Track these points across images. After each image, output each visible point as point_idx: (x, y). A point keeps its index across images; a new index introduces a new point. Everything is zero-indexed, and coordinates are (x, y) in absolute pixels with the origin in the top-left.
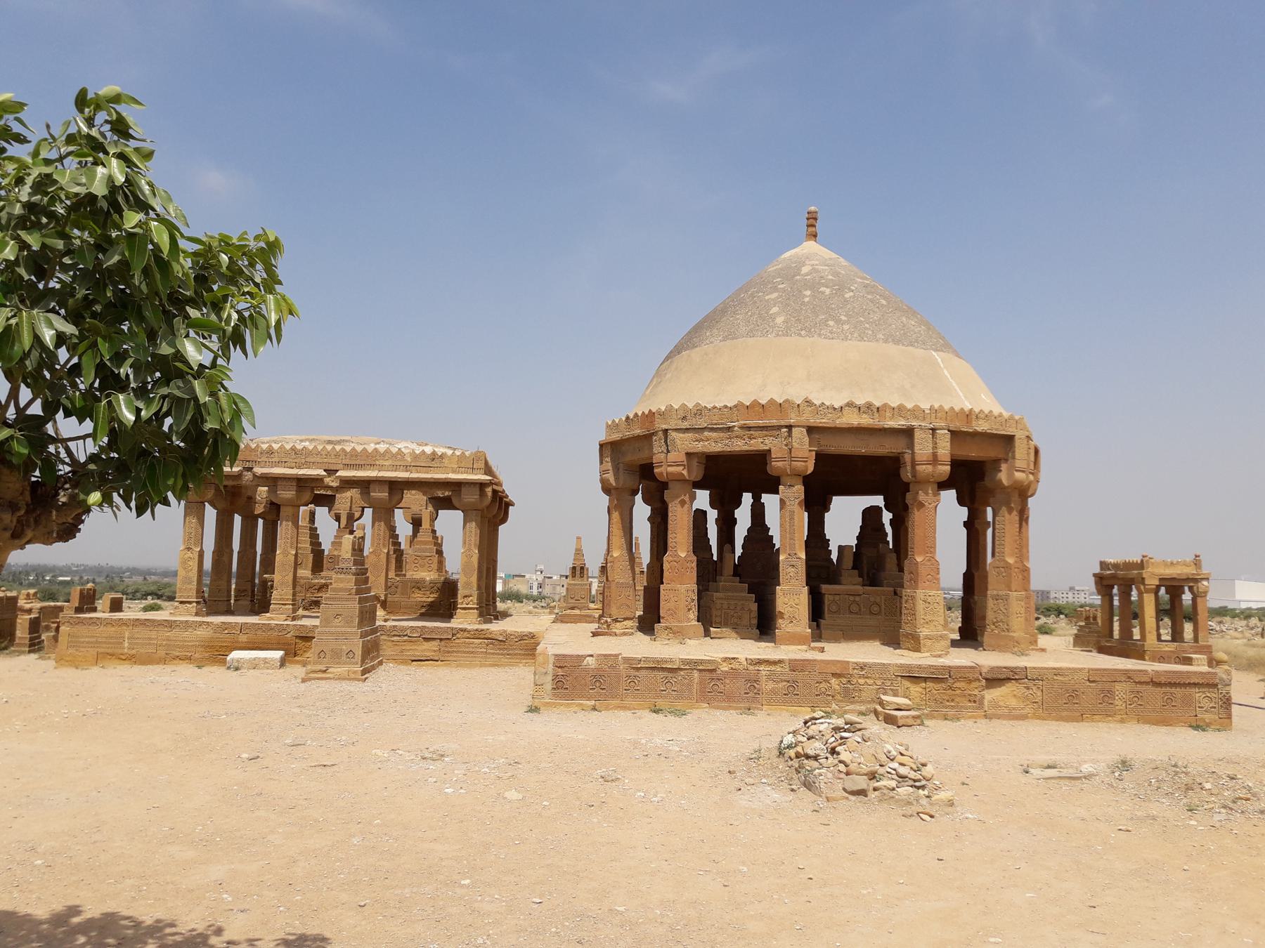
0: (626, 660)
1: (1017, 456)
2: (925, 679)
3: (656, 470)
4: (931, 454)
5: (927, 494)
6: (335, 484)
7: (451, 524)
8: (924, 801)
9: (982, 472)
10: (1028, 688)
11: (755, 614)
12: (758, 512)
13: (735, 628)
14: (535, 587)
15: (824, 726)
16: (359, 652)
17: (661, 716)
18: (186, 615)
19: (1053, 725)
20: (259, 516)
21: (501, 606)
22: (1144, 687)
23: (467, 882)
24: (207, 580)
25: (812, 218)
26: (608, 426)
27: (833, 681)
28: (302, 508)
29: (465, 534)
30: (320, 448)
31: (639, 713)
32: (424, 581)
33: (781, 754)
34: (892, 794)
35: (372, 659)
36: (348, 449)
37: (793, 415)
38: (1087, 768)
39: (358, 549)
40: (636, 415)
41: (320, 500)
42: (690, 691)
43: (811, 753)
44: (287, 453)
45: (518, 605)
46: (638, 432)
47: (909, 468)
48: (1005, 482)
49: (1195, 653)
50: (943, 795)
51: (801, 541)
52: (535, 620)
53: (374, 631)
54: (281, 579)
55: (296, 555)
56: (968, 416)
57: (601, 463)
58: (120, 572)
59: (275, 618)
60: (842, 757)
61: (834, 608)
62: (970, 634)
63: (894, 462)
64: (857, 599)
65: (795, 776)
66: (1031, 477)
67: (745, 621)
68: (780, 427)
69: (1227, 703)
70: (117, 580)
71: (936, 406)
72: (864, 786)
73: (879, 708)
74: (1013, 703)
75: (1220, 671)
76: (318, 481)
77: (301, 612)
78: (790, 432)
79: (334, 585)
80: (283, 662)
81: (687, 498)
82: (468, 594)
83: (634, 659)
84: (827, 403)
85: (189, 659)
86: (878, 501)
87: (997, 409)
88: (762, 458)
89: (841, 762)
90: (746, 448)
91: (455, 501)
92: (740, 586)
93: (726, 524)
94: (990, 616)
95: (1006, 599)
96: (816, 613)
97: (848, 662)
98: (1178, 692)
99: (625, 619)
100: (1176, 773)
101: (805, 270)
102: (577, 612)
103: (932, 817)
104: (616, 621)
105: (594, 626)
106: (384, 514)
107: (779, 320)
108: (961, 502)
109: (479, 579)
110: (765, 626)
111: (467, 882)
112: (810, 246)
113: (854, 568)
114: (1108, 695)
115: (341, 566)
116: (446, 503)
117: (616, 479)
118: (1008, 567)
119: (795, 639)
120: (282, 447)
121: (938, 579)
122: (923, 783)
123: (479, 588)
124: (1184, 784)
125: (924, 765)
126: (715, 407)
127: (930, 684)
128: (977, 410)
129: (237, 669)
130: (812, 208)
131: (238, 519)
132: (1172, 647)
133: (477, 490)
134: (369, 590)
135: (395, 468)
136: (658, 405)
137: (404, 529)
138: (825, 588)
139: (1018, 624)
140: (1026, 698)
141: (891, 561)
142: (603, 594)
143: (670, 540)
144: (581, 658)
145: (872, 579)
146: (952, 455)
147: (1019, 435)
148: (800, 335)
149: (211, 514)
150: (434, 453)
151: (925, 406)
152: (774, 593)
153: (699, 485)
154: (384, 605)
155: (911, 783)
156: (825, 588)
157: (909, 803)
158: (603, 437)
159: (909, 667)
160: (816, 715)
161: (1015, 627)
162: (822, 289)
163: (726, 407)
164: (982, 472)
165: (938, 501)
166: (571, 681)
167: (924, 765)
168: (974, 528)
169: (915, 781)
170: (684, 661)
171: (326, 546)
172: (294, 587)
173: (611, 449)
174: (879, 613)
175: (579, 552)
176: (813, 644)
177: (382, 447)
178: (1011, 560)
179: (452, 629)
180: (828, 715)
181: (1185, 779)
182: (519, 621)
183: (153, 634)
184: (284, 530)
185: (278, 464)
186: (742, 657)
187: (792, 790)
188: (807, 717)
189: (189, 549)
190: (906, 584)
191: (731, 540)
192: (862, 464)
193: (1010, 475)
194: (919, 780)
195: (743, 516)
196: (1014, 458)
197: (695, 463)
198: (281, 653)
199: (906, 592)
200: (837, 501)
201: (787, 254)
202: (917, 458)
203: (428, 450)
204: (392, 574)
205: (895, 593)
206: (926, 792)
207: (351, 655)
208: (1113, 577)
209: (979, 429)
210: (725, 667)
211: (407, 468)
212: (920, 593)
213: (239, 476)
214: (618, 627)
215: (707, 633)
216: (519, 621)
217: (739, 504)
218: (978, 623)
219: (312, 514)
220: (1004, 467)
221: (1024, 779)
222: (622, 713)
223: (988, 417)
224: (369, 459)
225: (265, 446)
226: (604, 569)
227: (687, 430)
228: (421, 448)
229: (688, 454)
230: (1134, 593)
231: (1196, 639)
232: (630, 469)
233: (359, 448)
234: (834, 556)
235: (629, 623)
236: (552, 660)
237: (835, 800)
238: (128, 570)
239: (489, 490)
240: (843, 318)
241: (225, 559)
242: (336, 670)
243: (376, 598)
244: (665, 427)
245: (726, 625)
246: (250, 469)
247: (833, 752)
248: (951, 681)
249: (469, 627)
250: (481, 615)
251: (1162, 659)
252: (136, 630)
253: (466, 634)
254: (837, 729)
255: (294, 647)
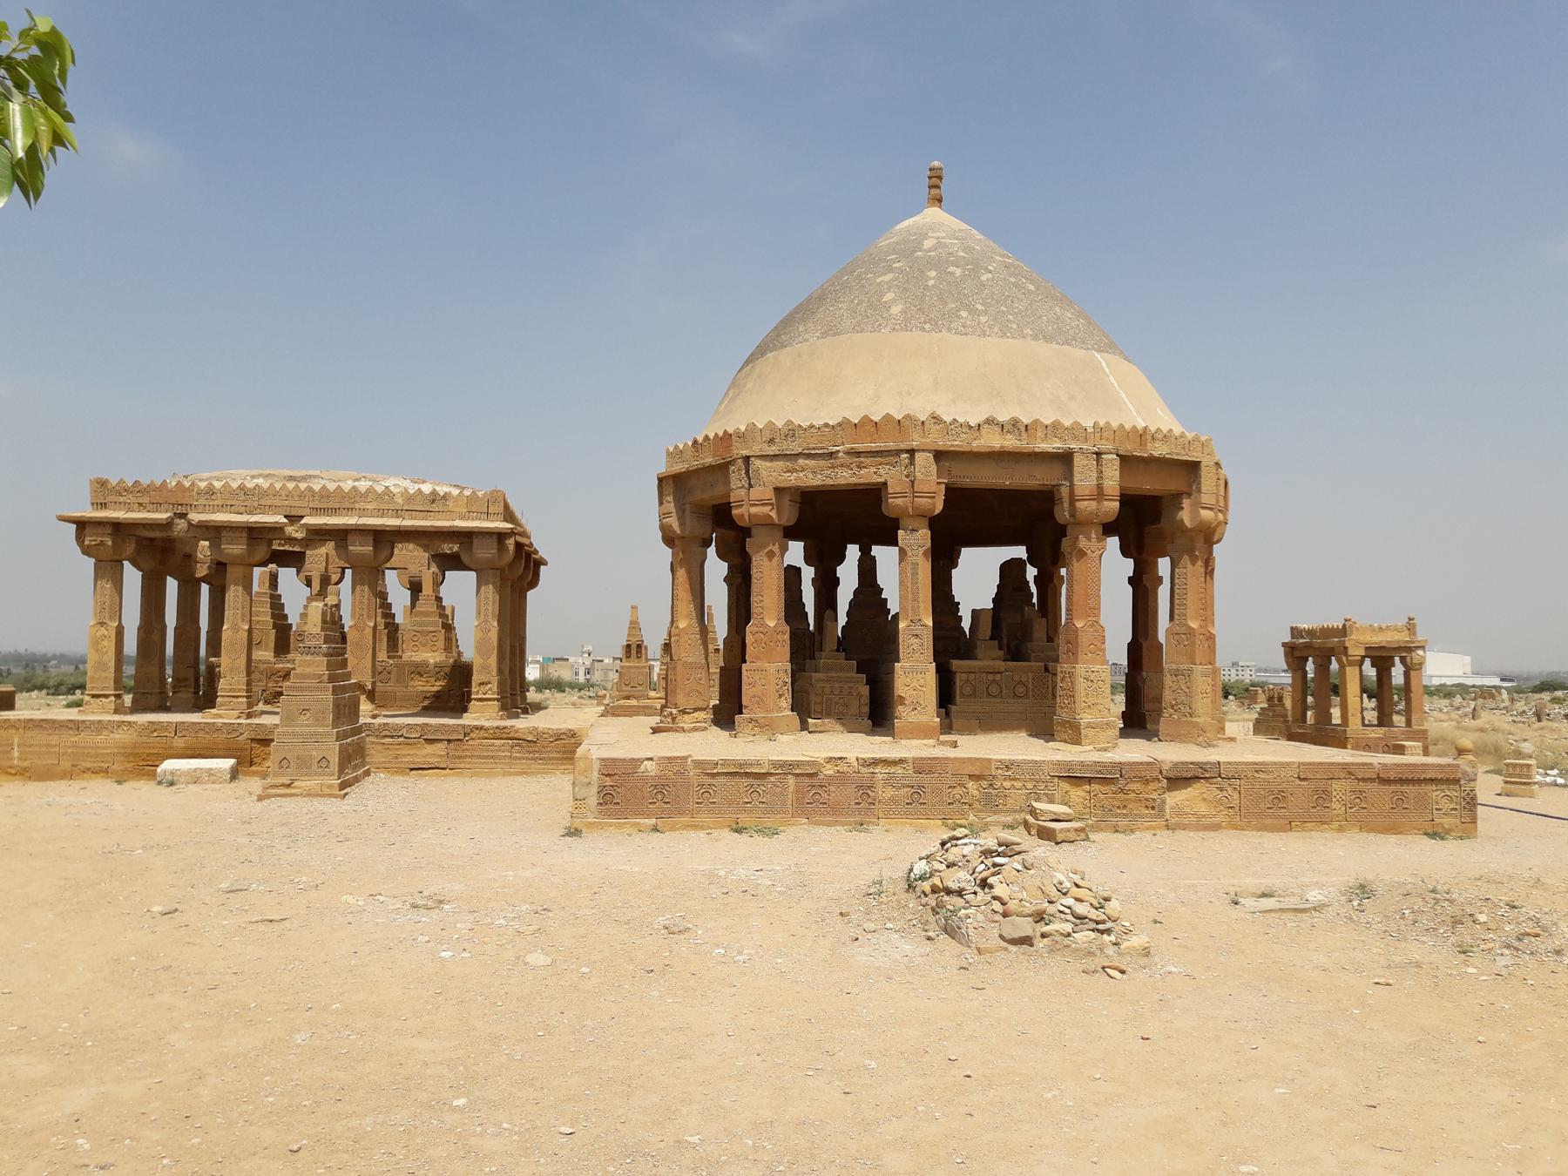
0: (697, 763)
1: (1204, 489)
2: (1090, 780)
3: (734, 512)
4: (1095, 487)
5: (1089, 539)
6: (299, 535)
7: (460, 589)
8: (1111, 951)
9: (1156, 514)
10: (1221, 790)
11: (866, 699)
12: (867, 569)
13: (840, 718)
14: (582, 673)
15: (968, 849)
16: (335, 760)
17: (744, 837)
18: (98, 712)
19: (1255, 837)
20: (203, 579)
21: (532, 695)
22: (1369, 786)
23: (461, 1102)
24: (130, 670)
25: (936, 177)
26: (669, 454)
27: (971, 785)
28: (257, 571)
29: (479, 601)
30: (278, 486)
31: (716, 833)
32: (426, 664)
33: (911, 887)
34: (1067, 941)
35: (355, 769)
36: (317, 487)
37: (915, 436)
38: (1315, 896)
39: (332, 621)
40: (707, 438)
41: (283, 559)
42: (784, 803)
43: (953, 886)
44: (233, 493)
45: (559, 695)
46: (709, 460)
47: (1066, 505)
48: (1188, 524)
49: (1408, 739)
50: (1136, 941)
51: (934, 599)
52: (578, 713)
53: (358, 731)
54: (230, 665)
55: (250, 631)
56: (1142, 436)
57: (661, 503)
58: (44, 660)
59: (223, 715)
60: (997, 891)
61: (968, 690)
62: (1137, 721)
63: (1046, 499)
64: (998, 677)
65: (932, 919)
66: (1221, 516)
67: (854, 710)
68: (898, 452)
69: (1471, 803)
70: (39, 671)
71: (1102, 423)
72: (1029, 932)
73: (1031, 819)
74: (1202, 808)
75: (1463, 762)
76: (276, 530)
77: (261, 707)
78: (912, 458)
79: (299, 670)
80: (234, 774)
81: (776, 549)
82: (486, 682)
83: (708, 762)
84: (961, 420)
85: (104, 772)
86: (1020, 552)
87: (1178, 429)
88: (876, 493)
89: (995, 898)
90: (854, 480)
91: (465, 558)
92: (847, 664)
93: (827, 586)
94: (1168, 696)
95: (1188, 674)
96: (946, 697)
97: (990, 760)
98: (1409, 789)
99: (696, 710)
100: (1437, 901)
101: (928, 244)
102: (633, 702)
103: (1123, 972)
104: (684, 712)
105: (655, 720)
106: (370, 575)
107: (896, 310)
108: (1125, 552)
109: (500, 660)
110: (879, 714)
111: (461, 1102)
112: (933, 214)
113: (992, 638)
114: (1323, 796)
115: (308, 644)
116: (452, 562)
117: (682, 524)
118: (1190, 633)
119: (920, 732)
120: (226, 485)
121: (1103, 650)
122: (1109, 925)
123: (500, 672)
124: (1451, 916)
125: (1107, 900)
126: (812, 426)
127: (1095, 787)
128: (1153, 429)
129: (172, 784)
130: (936, 164)
131: (172, 585)
132: (1380, 732)
133: (494, 542)
134: (348, 676)
135: (382, 513)
136: (736, 422)
137: (399, 597)
138: (956, 664)
139: (1203, 705)
140: (1220, 802)
141: (1039, 628)
142: (666, 679)
143: (754, 605)
144: (636, 762)
145: (1016, 653)
146: (1121, 488)
147: (1206, 461)
148: (923, 329)
149: (132, 578)
150: (434, 492)
151: (1088, 423)
152: (892, 672)
153: (791, 533)
154: (371, 696)
155: (1093, 925)
156: (956, 664)
157: (1091, 954)
158: (662, 467)
159: (1068, 765)
160: (958, 833)
161: (1201, 711)
162: (952, 269)
163: (827, 425)
164: (1156, 514)
165: (1104, 548)
166: (624, 794)
167: (1107, 900)
168: (1143, 585)
169: (1097, 923)
170: (775, 764)
171: (293, 619)
172: (249, 672)
173: (674, 485)
174: (1026, 696)
175: (634, 626)
176: (943, 738)
177: (363, 485)
178: (1194, 625)
179: (464, 726)
180: (975, 833)
181: (1450, 910)
182: (557, 716)
183: (54, 740)
184: (234, 595)
185: (221, 508)
186: (852, 756)
187: (929, 938)
188: (945, 837)
189: (102, 624)
190: (1062, 657)
191: (833, 605)
192: (1008, 504)
193: (1195, 514)
194: (1103, 922)
195: (848, 574)
196: (1199, 491)
197: (786, 500)
198: (231, 762)
199: (1062, 667)
200: (968, 555)
201: (905, 224)
202: (1078, 492)
203: (426, 488)
204: (382, 655)
205: (1047, 670)
206: (1112, 938)
207: (324, 764)
208: (1308, 646)
209: (1156, 454)
210: (829, 770)
211: (397, 513)
212: (1080, 669)
213: (168, 525)
214: (686, 721)
215: (804, 726)
216: (557, 716)
217: (842, 559)
218: (1147, 706)
219: (274, 578)
220: (1186, 503)
221: (1235, 913)
222: (693, 834)
223: (1166, 438)
224: (348, 500)
225: (203, 485)
226: (667, 647)
227: (775, 457)
228: (417, 487)
229: (776, 489)
230: (1334, 666)
231: (1409, 723)
232: (699, 511)
233: (331, 487)
234: (966, 624)
235: (701, 715)
236: (596, 766)
237: (988, 951)
238: (54, 657)
239: (510, 543)
240: (980, 307)
241: (156, 637)
242: (304, 784)
243: (360, 687)
244: (746, 452)
245: (829, 715)
246: (183, 516)
247: (984, 884)
248: (1122, 781)
249: (487, 724)
250: (503, 708)
251: (1368, 747)
252: (29, 734)
253: (482, 734)
254: (987, 853)
255: (249, 754)
